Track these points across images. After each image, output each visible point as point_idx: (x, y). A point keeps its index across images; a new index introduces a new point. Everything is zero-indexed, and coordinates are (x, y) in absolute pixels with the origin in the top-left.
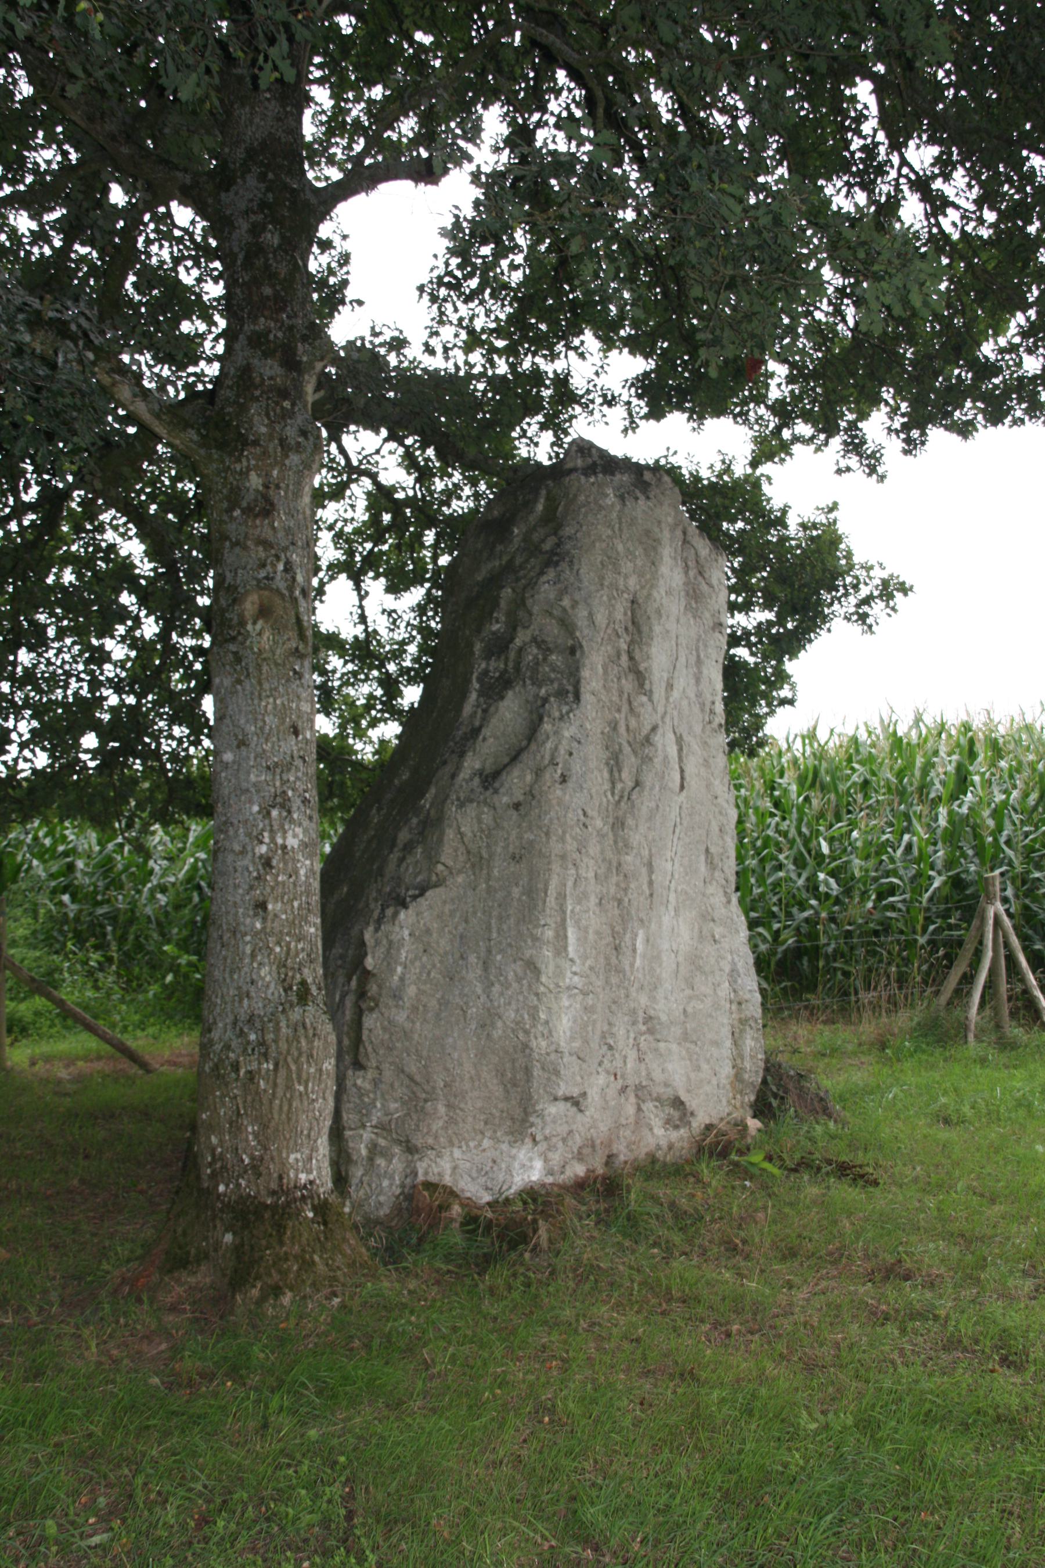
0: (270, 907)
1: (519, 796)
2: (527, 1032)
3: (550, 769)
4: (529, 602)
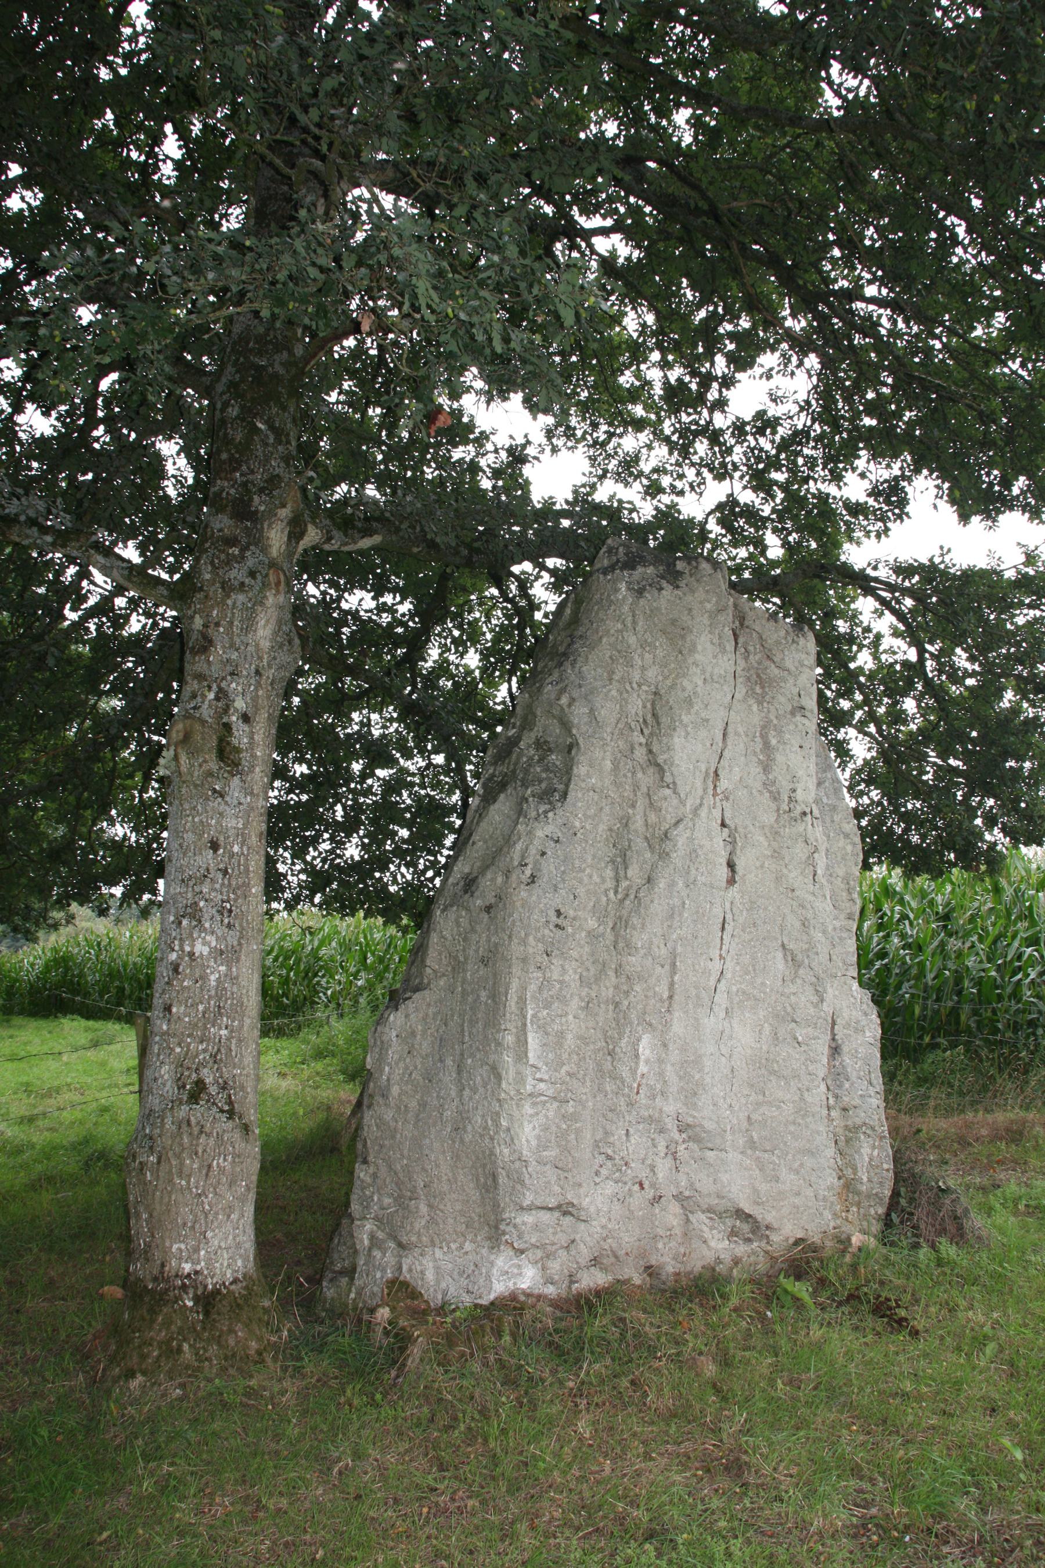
2: (492, 1139)
3: (518, 871)
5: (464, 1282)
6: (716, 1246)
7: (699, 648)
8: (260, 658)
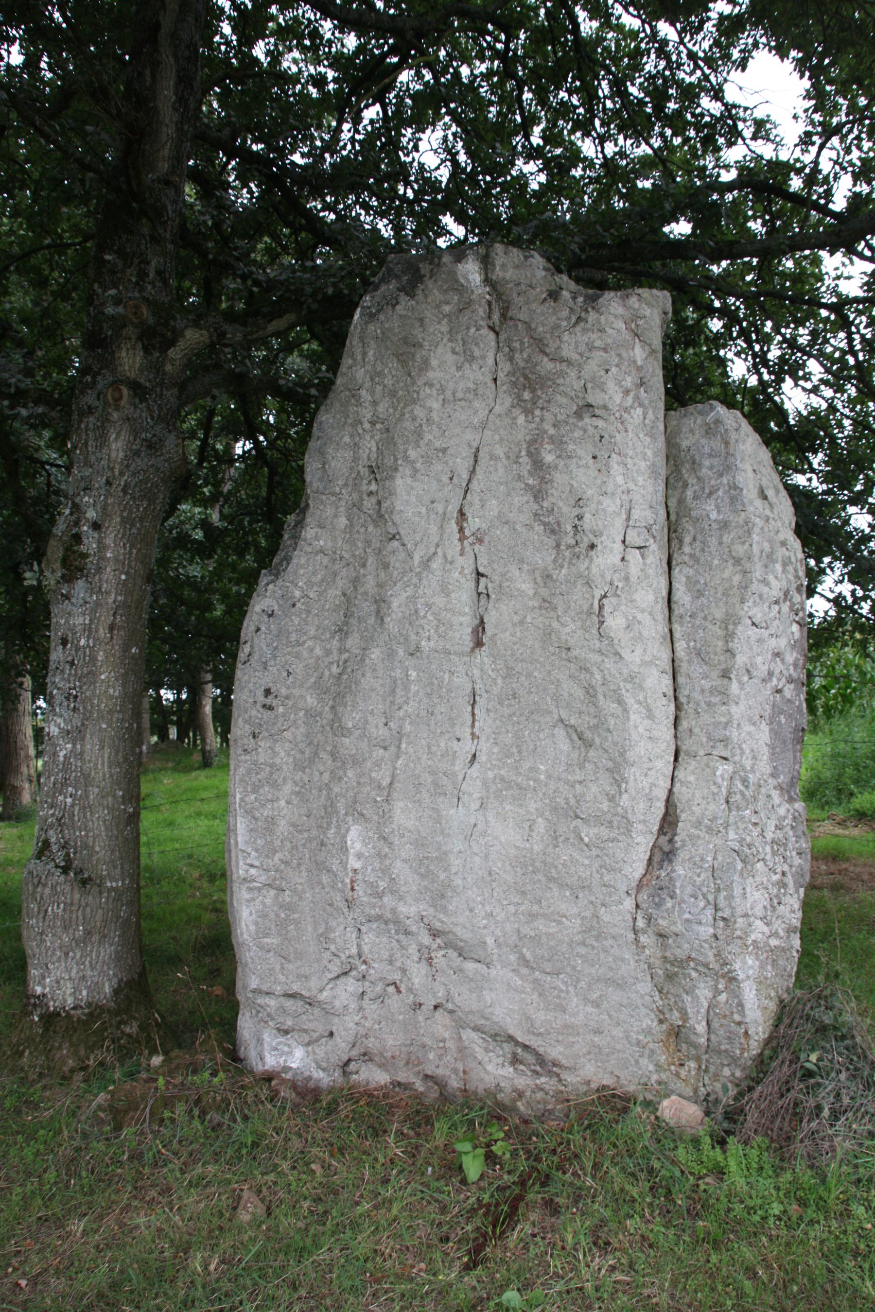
6: (494, 1072)
7: (434, 363)
8: (112, 469)
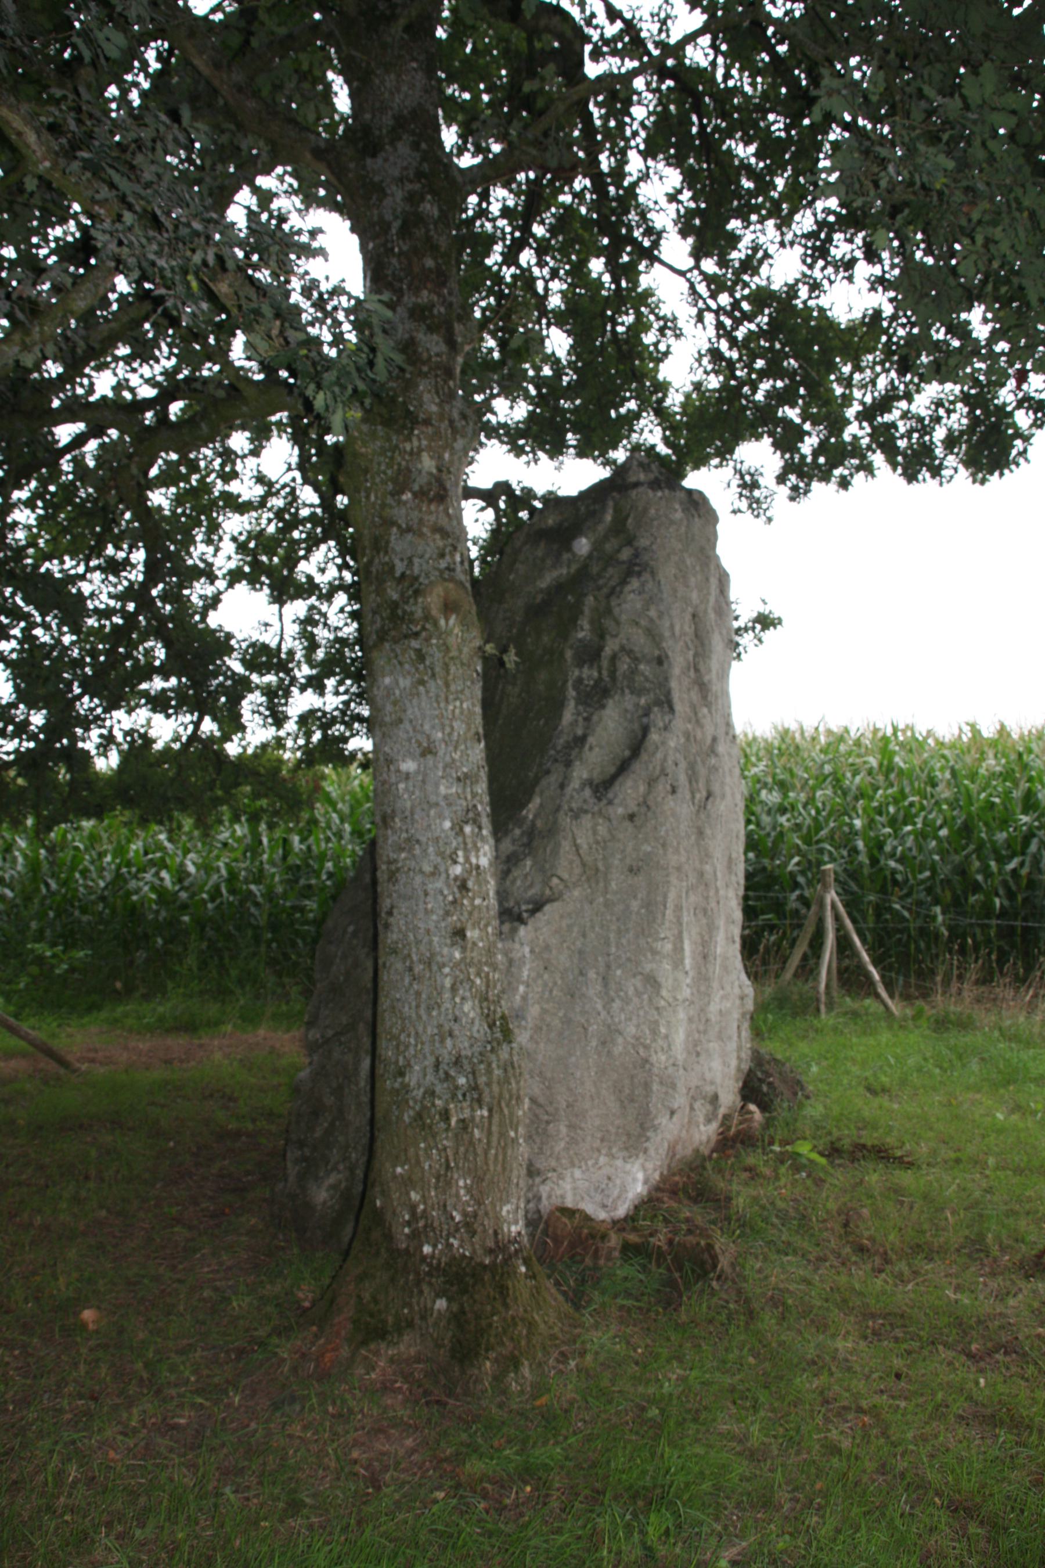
0: (469, 934)
1: (633, 807)
3: (662, 779)
4: (616, 611)
5: (598, 1198)
